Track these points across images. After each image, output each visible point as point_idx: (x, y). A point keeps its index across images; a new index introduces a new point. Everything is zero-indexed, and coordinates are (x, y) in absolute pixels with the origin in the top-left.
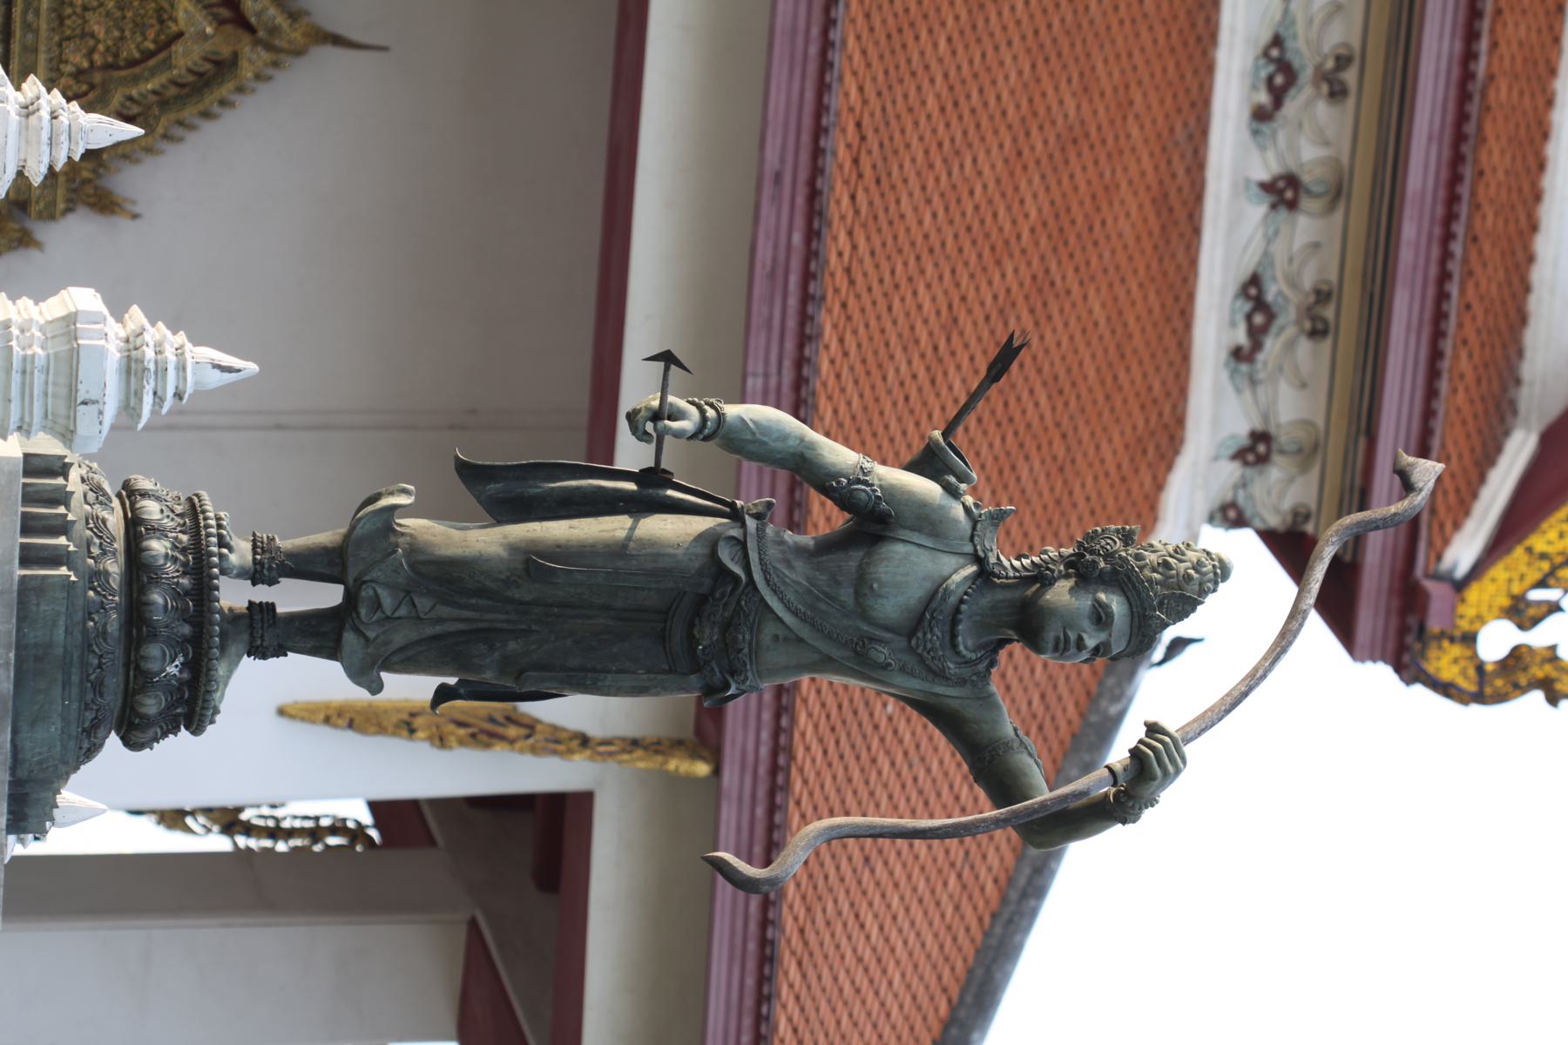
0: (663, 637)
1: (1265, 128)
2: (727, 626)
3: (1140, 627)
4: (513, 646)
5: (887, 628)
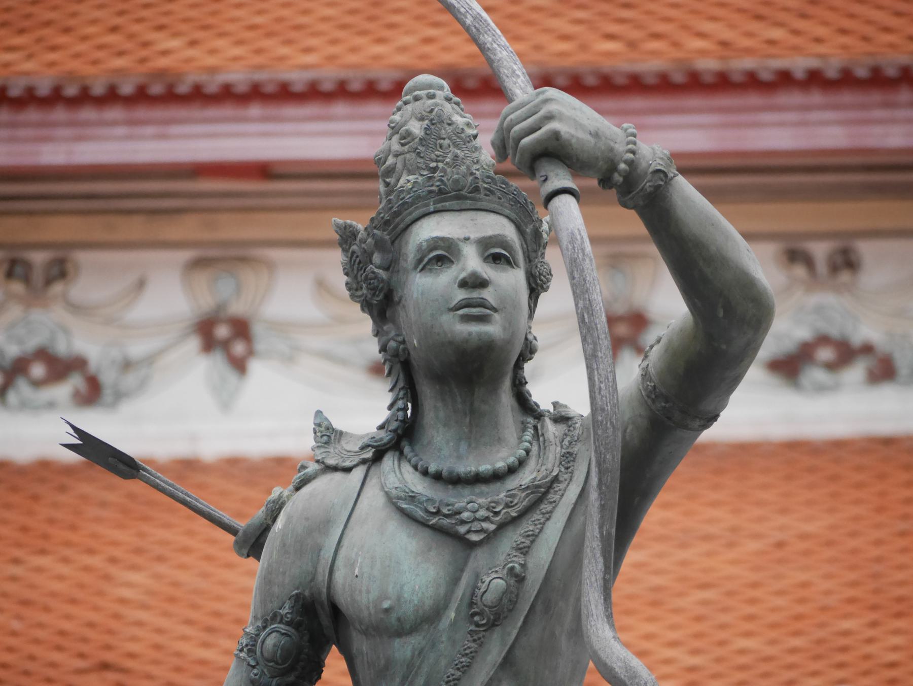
3: (459, 198)
5: (455, 581)
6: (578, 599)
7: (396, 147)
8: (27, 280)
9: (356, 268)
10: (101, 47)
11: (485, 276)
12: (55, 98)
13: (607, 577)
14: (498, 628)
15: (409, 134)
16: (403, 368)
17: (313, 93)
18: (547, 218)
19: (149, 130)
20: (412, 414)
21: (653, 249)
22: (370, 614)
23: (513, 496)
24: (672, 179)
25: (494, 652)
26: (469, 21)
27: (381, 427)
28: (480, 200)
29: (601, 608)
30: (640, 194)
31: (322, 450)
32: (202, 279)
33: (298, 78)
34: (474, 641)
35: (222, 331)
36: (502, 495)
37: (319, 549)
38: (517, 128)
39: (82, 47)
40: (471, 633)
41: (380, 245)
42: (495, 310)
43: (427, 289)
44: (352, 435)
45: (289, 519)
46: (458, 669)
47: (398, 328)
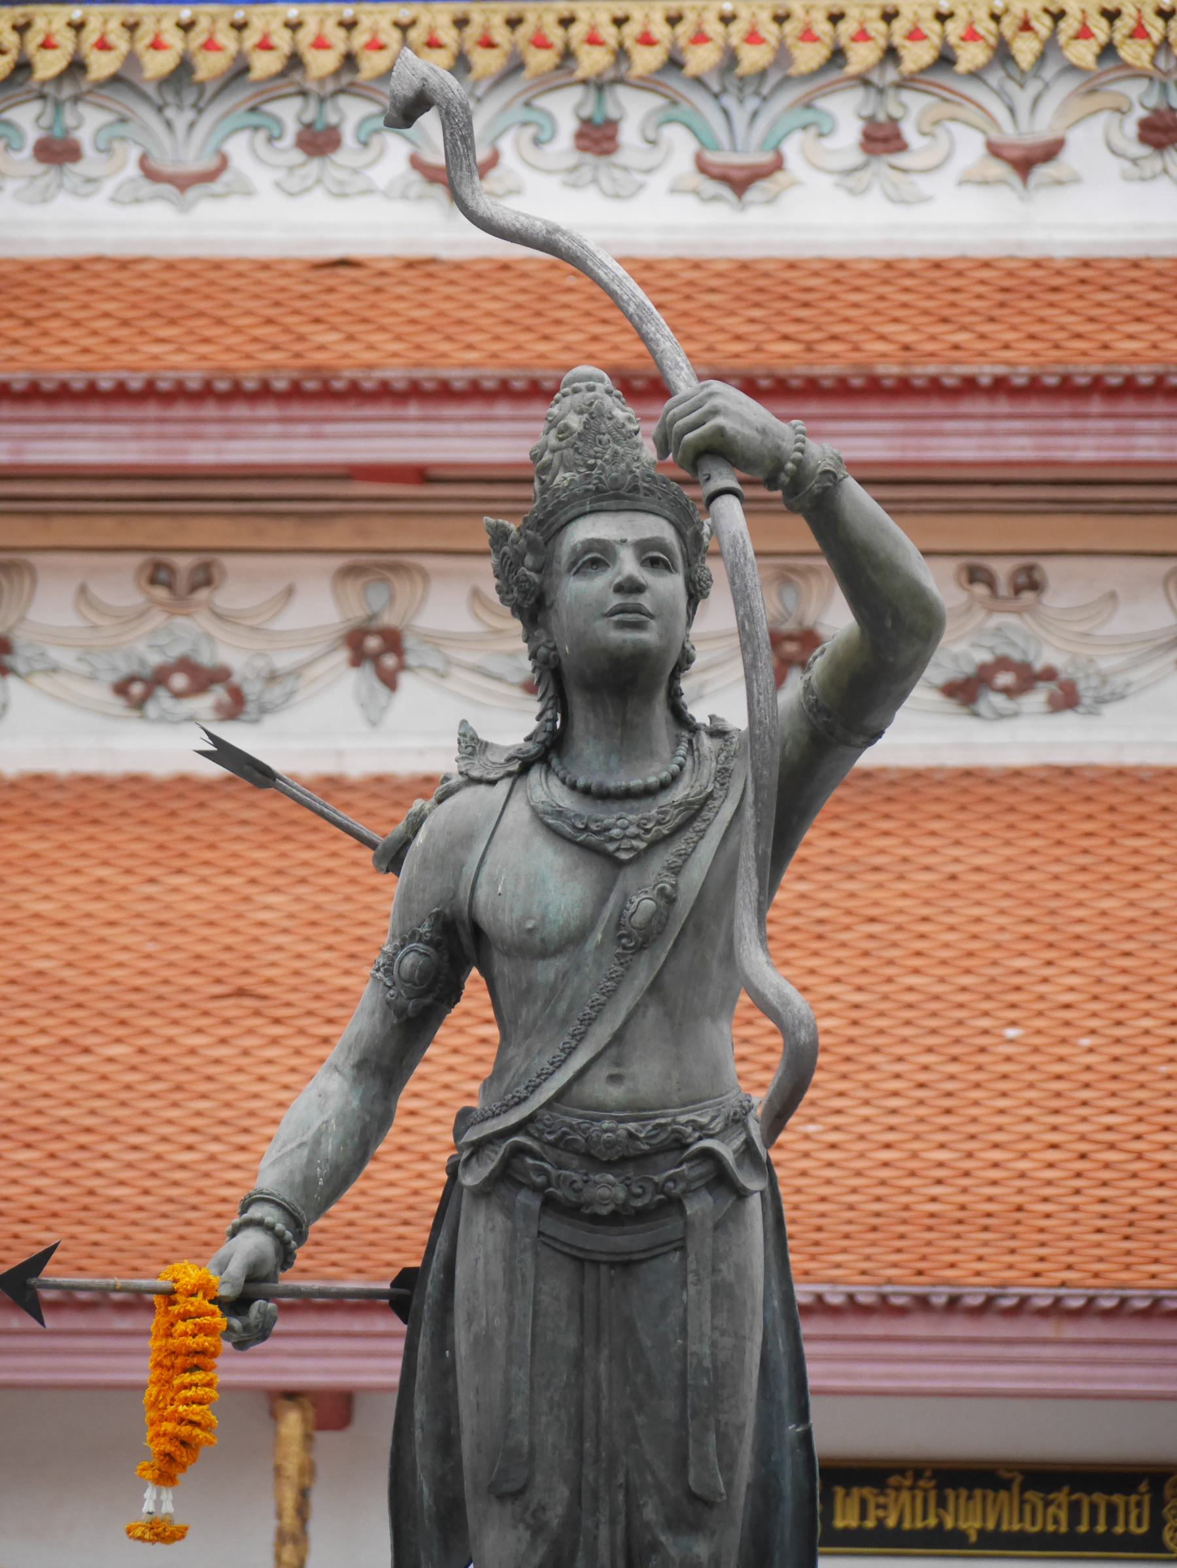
0: (626, 1265)
1: (1086, 689)
2: (594, 1158)
3: (617, 497)
4: (650, 1512)
5: (602, 901)
6: (731, 923)
7: (553, 441)
8: (169, 586)
9: (507, 572)
10: (256, 340)
11: (642, 580)
12: (206, 393)
13: (762, 898)
14: (646, 951)
15: (567, 428)
16: (554, 679)
17: (475, 392)
18: (709, 520)
19: (303, 428)
20: (561, 725)
21: (823, 562)
22: (513, 934)
23: (665, 813)
24: (841, 480)
25: (642, 977)
26: (632, 309)
27: (528, 739)
28: (639, 500)
29: (754, 931)
30: (806, 496)
31: (467, 761)
32: (352, 587)
33: (458, 377)
34: (621, 964)
35: (373, 643)
36: (654, 812)
37: (462, 865)
38: (680, 423)
39: (234, 340)
40: (618, 956)
41: (532, 546)
42: (651, 616)
43: (582, 592)
44: (497, 747)
45: (431, 832)
46: (603, 994)
47: (549, 633)
